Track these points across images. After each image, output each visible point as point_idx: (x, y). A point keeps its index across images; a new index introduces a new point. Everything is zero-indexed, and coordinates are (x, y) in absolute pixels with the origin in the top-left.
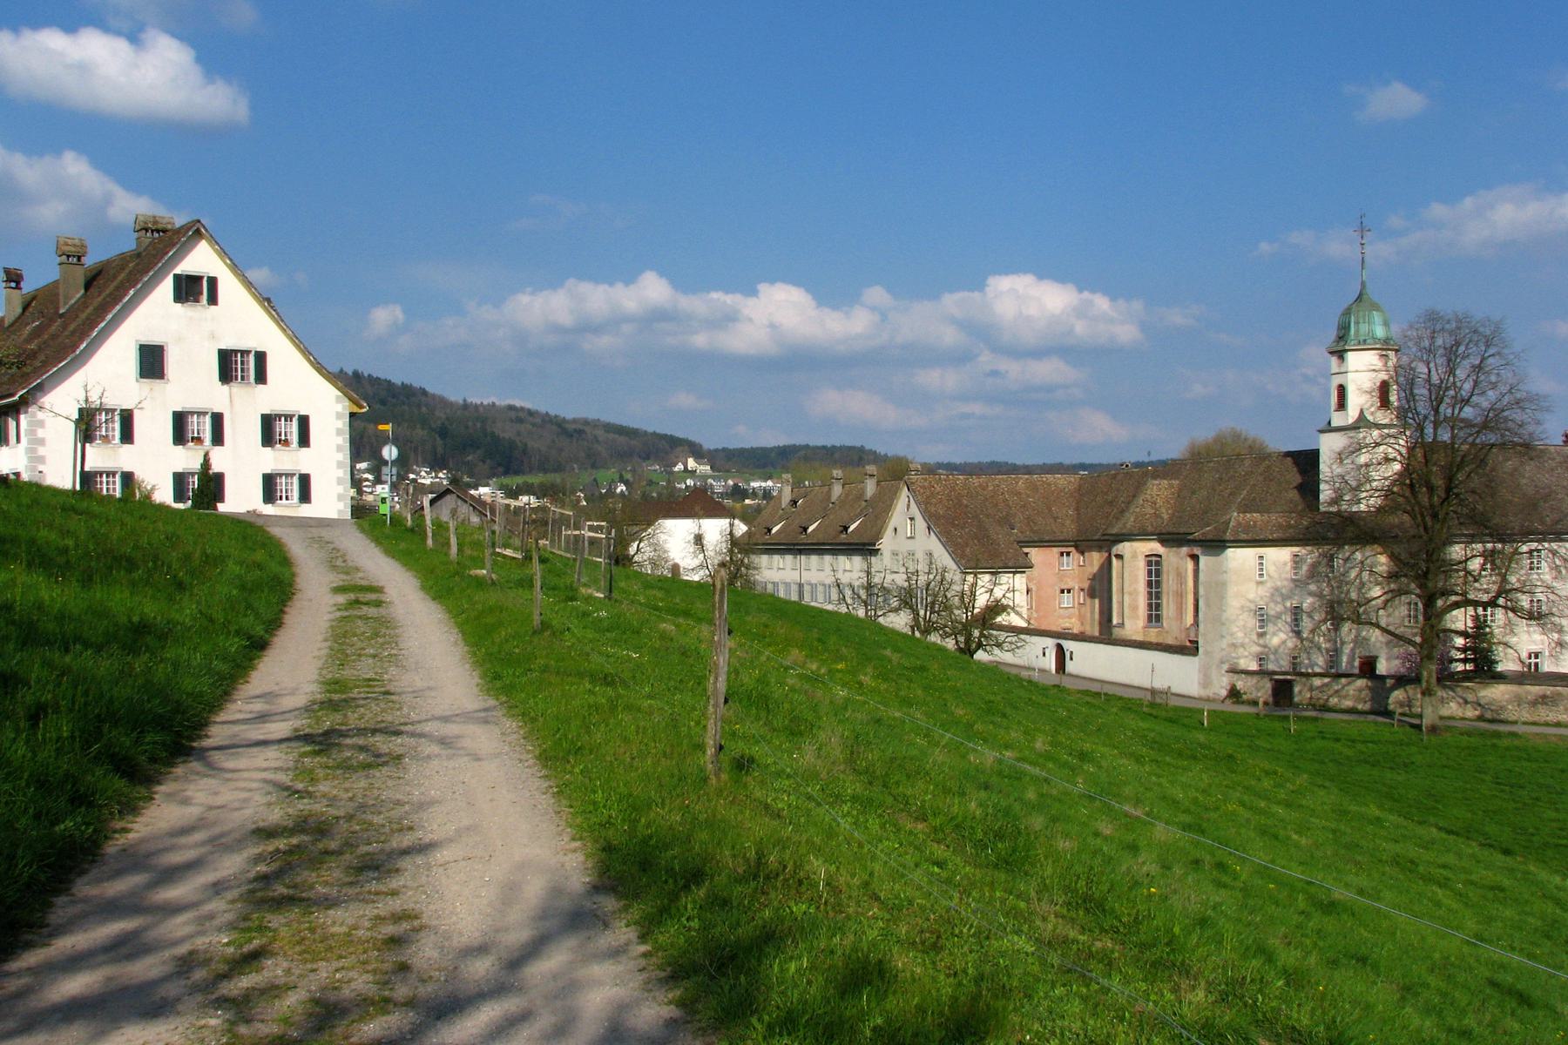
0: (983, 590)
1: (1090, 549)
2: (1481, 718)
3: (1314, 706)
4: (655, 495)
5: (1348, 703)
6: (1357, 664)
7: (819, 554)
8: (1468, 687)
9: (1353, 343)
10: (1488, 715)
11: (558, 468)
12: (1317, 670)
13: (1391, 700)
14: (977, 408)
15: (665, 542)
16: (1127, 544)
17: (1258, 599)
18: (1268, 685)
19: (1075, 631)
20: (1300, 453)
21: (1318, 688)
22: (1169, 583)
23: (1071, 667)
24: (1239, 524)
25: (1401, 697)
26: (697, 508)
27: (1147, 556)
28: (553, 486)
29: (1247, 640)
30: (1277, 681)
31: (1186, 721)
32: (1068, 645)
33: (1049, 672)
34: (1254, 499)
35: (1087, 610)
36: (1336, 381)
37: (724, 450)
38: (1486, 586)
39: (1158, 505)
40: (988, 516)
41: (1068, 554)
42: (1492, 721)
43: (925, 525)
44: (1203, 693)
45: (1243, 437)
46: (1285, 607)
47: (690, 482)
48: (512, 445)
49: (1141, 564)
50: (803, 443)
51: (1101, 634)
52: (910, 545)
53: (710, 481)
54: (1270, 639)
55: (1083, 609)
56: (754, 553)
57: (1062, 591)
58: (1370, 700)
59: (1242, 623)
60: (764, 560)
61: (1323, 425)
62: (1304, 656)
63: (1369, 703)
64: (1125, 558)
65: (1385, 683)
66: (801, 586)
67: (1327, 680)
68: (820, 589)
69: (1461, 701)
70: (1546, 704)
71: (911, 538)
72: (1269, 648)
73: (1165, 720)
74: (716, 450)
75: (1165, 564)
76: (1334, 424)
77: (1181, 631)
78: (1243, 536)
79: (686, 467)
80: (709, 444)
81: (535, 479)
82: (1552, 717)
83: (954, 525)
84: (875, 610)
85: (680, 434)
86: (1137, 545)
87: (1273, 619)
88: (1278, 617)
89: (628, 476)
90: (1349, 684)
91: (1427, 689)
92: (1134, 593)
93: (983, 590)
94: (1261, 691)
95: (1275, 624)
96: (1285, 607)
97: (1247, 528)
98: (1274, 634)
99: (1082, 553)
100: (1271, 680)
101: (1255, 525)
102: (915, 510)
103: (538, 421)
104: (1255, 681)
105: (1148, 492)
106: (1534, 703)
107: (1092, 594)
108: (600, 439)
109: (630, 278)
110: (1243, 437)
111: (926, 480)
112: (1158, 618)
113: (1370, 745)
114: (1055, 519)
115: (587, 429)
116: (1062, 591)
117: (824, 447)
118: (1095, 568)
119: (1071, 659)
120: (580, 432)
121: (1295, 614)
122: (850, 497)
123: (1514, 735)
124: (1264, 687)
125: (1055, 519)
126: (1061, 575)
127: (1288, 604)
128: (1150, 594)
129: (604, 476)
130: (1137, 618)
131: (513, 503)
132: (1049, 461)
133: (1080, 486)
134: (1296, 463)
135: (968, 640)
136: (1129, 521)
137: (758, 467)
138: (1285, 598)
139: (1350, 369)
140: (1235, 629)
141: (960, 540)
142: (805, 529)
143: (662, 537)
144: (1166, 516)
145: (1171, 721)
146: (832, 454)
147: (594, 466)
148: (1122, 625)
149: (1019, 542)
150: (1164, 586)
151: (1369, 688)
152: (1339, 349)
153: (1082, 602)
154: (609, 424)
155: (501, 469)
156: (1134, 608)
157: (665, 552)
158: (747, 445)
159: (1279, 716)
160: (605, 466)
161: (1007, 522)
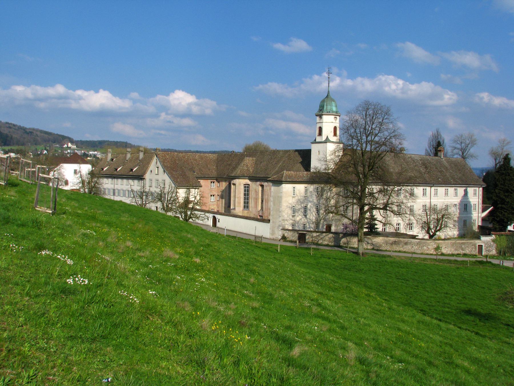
0: (192, 196)
1: (222, 181)
2: (373, 249)
4: (57, 155)
5: (326, 243)
6: (325, 227)
8: (369, 238)
10: (376, 248)
11: (23, 144)
12: (312, 230)
13: (341, 242)
15: (64, 172)
16: (237, 180)
18: (297, 235)
19: (216, 211)
20: (301, 150)
21: (314, 237)
22: (252, 194)
23: (218, 225)
26: (79, 161)
28: (21, 150)
30: (300, 233)
31: (270, 249)
32: (218, 217)
34: (285, 166)
36: (318, 125)
37: (81, 141)
38: (381, 201)
40: (185, 167)
41: (214, 182)
42: (377, 250)
44: (271, 237)
47: (69, 151)
48: (7, 136)
49: (242, 187)
52: (157, 177)
53: (76, 151)
55: (218, 202)
56: (101, 178)
60: (105, 180)
62: (307, 224)
64: (236, 185)
65: (339, 235)
68: (121, 191)
70: (396, 244)
74: (78, 141)
76: (317, 141)
78: (288, 180)
79: (68, 146)
80: (76, 138)
81: (15, 148)
82: (398, 249)
83: (174, 171)
84: (146, 201)
85: (66, 135)
88: (299, 210)
89: (48, 148)
91: (361, 239)
94: (294, 237)
95: (298, 213)
97: (290, 177)
98: (298, 216)
99: (219, 182)
100: (298, 233)
102: (159, 164)
103: (17, 128)
106: (392, 244)
107: (222, 197)
108: (39, 135)
109: (53, 85)
110: (262, 144)
111: (163, 153)
112: (248, 207)
113: (342, 261)
114: (209, 169)
115: (34, 132)
116: (211, 196)
117: (114, 142)
118: (224, 188)
119: (219, 222)
120: (31, 133)
121: (305, 209)
123: (389, 256)
125: (209, 169)
126: (211, 190)
127: (303, 205)
128: (245, 198)
129: (39, 148)
131: (450, 179)
133: (218, 158)
134: (299, 154)
135: (186, 215)
136: (238, 172)
137: (92, 147)
138: (302, 203)
139: (324, 121)
142: (116, 170)
143: (63, 170)
144: (251, 171)
145: (265, 249)
147: (36, 144)
148: (234, 209)
150: (250, 196)
151: (334, 237)
153: (218, 199)
154: (42, 130)
155: (3, 144)
156: (239, 203)
157: (64, 176)
158: (88, 140)
160: (40, 144)
161: (192, 170)
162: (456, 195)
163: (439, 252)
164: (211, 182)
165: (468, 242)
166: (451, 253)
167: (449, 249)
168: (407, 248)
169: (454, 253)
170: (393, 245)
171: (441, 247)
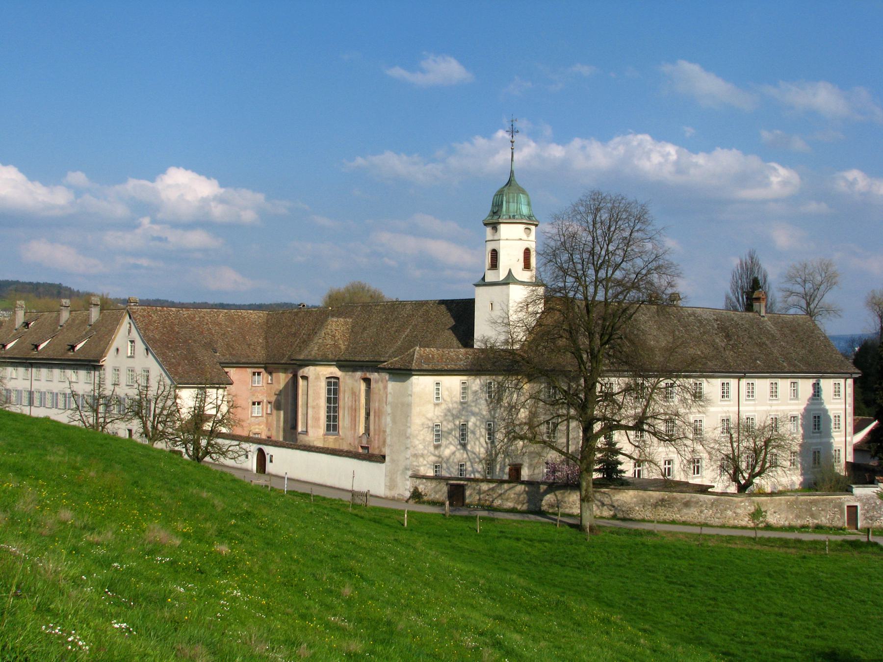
0: (211, 406)
1: (277, 370)
2: (614, 517)
3: (483, 506)
5: (509, 505)
6: (507, 470)
7: (61, 369)
8: (604, 493)
9: (505, 217)
10: (620, 515)
12: (478, 476)
13: (543, 503)
14: (144, 262)
16: (311, 368)
17: (435, 418)
18: (445, 489)
19: (264, 437)
20: (452, 301)
21: (485, 492)
22: (345, 400)
23: (270, 468)
24: (421, 356)
25: (552, 500)
27: (327, 378)
29: (426, 452)
30: (452, 485)
31: (387, 521)
33: (252, 471)
35: (273, 418)
36: (490, 246)
38: (630, 410)
39: (336, 338)
40: (195, 341)
41: (259, 374)
42: (624, 519)
43: (144, 347)
44: (389, 494)
45: (366, 288)
46: (455, 425)
49: (323, 384)
50: (15, 279)
51: (285, 438)
52: (131, 363)
54: (444, 451)
55: (270, 418)
57: (254, 404)
58: (527, 502)
59: (422, 437)
61: (478, 279)
62: (468, 464)
63: (527, 504)
64: (310, 379)
65: (539, 488)
66: (31, 393)
67: (492, 485)
68: (48, 396)
69: (599, 504)
70: (665, 506)
71: (130, 357)
72: (443, 459)
73: (370, 520)
75: (342, 385)
76: (487, 280)
77: (354, 439)
78: (425, 367)
82: (669, 516)
83: (168, 348)
86: (319, 369)
87: (446, 434)
90: (510, 489)
91: (586, 496)
92: (316, 407)
93: (211, 406)
94: (440, 492)
95: (447, 439)
96: (455, 425)
97: (428, 360)
98: (446, 447)
99: (270, 373)
100: (447, 484)
101: (433, 357)
102: (135, 334)
104: (434, 485)
105: (329, 327)
106: (655, 505)
107: (277, 406)
110: (366, 288)
111: (144, 310)
113: (546, 544)
114: (249, 345)
116: (254, 404)
117: (31, 283)
119: (271, 461)
121: (462, 430)
122: (77, 322)
123: (650, 533)
124: (440, 491)
125: (249, 345)
127: (457, 423)
130: (319, 427)
132: (199, 300)
133: (268, 320)
134: (449, 309)
135: (197, 448)
136: (314, 350)
138: (455, 417)
140: (417, 442)
141: (173, 360)
142: (37, 347)
145: (375, 522)
146: (37, 289)
149: (221, 363)
150: (341, 403)
152: (494, 221)
156: (317, 419)
159: (461, 517)
161: (210, 346)
162: (795, 395)
163: (762, 522)
164: (254, 374)
165: (823, 500)
166: (787, 523)
167: (783, 516)
168: (691, 514)
169: (793, 523)
170: (659, 507)
171: (766, 512)
